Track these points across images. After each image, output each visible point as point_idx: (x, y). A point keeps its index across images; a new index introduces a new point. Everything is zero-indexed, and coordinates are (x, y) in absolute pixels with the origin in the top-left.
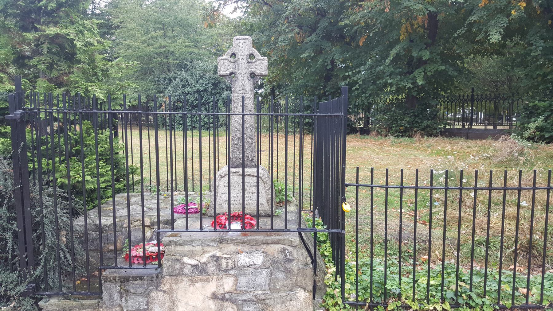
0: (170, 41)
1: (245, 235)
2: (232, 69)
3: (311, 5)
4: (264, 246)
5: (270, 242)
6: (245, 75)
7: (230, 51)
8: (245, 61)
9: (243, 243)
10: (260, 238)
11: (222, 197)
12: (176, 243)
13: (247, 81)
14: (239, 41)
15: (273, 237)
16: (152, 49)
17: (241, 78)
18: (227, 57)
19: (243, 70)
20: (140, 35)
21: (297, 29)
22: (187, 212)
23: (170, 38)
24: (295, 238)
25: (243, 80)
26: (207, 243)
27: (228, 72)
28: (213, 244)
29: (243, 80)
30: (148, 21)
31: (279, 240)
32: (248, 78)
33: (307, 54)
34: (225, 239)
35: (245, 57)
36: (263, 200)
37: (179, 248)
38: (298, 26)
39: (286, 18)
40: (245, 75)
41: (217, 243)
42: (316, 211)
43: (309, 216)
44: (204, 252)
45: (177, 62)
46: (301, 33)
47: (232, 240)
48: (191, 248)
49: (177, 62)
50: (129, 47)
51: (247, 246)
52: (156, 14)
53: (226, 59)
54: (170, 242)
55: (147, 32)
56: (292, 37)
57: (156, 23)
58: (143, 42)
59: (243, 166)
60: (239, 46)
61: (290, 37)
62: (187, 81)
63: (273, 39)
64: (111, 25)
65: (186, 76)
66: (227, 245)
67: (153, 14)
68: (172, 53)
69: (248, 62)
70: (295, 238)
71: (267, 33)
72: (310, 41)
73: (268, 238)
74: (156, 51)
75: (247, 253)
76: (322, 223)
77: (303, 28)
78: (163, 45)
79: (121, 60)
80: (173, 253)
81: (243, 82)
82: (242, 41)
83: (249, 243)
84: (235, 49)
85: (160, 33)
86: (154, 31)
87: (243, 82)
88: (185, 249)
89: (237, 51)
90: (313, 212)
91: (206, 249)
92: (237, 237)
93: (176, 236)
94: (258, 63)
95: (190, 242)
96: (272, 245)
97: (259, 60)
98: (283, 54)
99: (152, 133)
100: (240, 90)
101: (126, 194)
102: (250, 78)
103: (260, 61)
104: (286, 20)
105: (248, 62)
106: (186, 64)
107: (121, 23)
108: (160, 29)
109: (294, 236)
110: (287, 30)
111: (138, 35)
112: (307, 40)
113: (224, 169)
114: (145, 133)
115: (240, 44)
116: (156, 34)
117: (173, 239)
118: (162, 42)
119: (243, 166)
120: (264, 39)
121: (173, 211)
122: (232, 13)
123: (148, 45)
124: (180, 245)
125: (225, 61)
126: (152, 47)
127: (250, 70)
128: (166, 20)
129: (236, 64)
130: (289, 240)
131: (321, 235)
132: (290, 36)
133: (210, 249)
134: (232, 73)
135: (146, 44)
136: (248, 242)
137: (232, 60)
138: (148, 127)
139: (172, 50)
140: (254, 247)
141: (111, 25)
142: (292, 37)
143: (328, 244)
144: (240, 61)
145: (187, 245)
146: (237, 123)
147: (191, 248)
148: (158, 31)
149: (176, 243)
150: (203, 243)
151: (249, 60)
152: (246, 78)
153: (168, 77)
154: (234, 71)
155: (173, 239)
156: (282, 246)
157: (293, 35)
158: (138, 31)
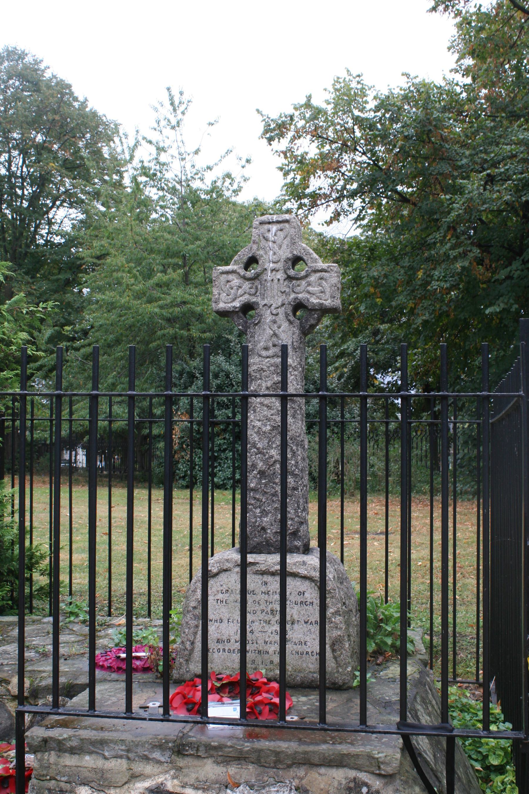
0: (195, 291)
1: (250, 736)
2: (247, 296)
3: (507, 197)
4: (301, 772)
5: (316, 760)
6: (281, 311)
7: (244, 254)
8: (280, 275)
9: (240, 758)
10: (287, 746)
11: (224, 626)
12: (61, 747)
13: (285, 325)
14: (266, 226)
15: (324, 747)
16: (157, 310)
17: (268, 318)
18: (235, 267)
19: (274, 298)
20: (132, 281)
21: (477, 251)
22: (127, 668)
23: (197, 285)
24: (388, 750)
25: (275, 322)
26: (141, 751)
27: (237, 304)
28: (157, 755)
29: (275, 322)
30: (152, 251)
31: (348, 755)
32: (287, 315)
33: (502, 306)
34: (190, 745)
35: (280, 265)
36: (304, 637)
37: (69, 761)
38: (479, 246)
39: (449, 228)
40: (281, 311)
41: (168, 753)
42: (492, 685)
43: (471, 698)
44: (135, 777)
45: (208, 335)
46: (487, 261)
47: (209, 747)
48: (100, 763)
49: (208, 335)
50: (111, 306)
51: (251, 767)
52: (169, 236)
53: (233, 272)
54: (45, 741)
55: (149, 274)
56: (463, 268)
57: (169, 253)
58: (138, 296)
59: (283, 551)
60: (266, 239)
61: (459, 270)
62: (227, 376)
63: (420, 274)
64: (81, 265)
65: (226, 366)
66: (196, 762)
67: (163, 236)
68: (200, 318)
69: (290, 278)
70: (390, 751)
71: (406, 262)
72: (509, 277)
73: (311, 748)
74: (164, 312)
75: (251, 787)
76: (502, 717)
77: (491, 249)
78: (179, 300)
79: (20, 301)
80: (52, 773)
81: (275, 327)
82: (274, 228)
83: (258, 759)
84: (255, 247)
85: (176, 275)
86: (162, 272)
87: (275, 327)
88: (84, 764)
89: (261, 252)
90: (485, 686)
91: (139, 767)
92: (223, 741)
93: (64, 725)
94: (313, 278)
95: (95, 747)
96: (323, 770)
97: (316, 271)
98: (445, 308)
99: (158, 494)
100: (266, 349)
101: (15, 619)
102: (292, 318)
103: (318, 275)
104: (451, 232)
105: (290, 278)
106: (228, 341)
107: (99, 258)
108: (176, 266)
109: (387, 745)
110: (453, 253)
111: (127, 279)
112: (502, 274)
113: (225, 554)
114: (140, 494)
115: (270, 236)
116: (165, 278)
117: (57, 733)
118: (178, 294)
119: (283, 551)
120: (400, 275)
121: (93, 665)
122: (329, 223)
123: (150, 302)
124: (72, 751)
125: (230, 277)
126: (156, 304)
127: (293, 296)
128: (191, 247)
129: (257, 283)
130: (370, 757)
131: (493, 750)
132: (458, 265)
133: (148, 769)
134: (247, 308)
135: (145, 299)
136: (254, 756)
137: (249, 274)
138: (149, 482)
139: (199, 309)
140: (272, 772)
141: (81, 265)
142: (463, 268)
143: (510, 777)
144: (269, 276)
145: (91, 753)
146: (258, 433)
147: (100, 763)
148: (170, 270)
149: (61, 747)
150: (130, 751)
151: (292, 272)
152: (281, 316)
153: (188, 369)
154: (254, 299)
155: (57, 733)
156: (352, 774)
157: (466, 264)
158: (129, 272)
